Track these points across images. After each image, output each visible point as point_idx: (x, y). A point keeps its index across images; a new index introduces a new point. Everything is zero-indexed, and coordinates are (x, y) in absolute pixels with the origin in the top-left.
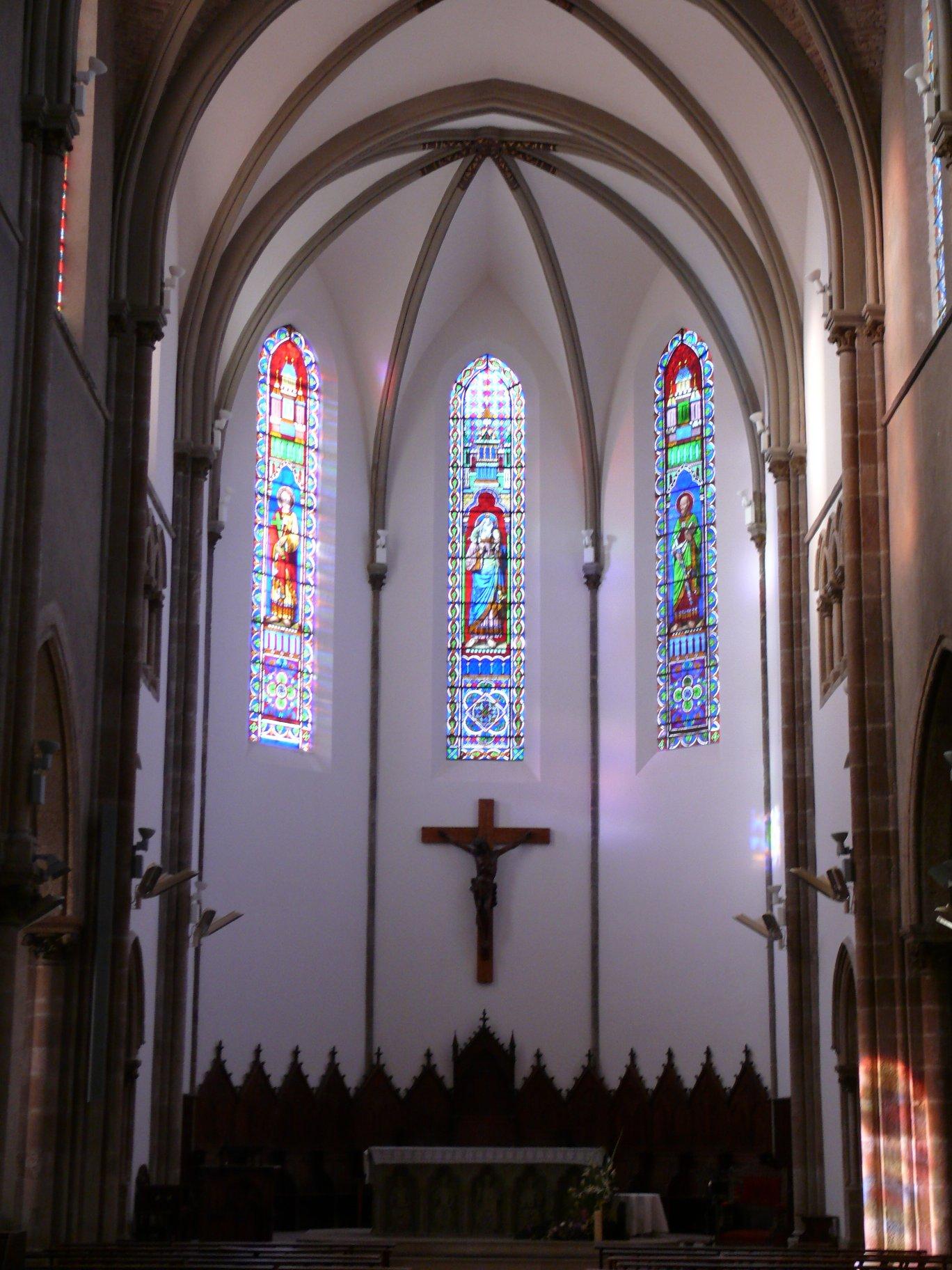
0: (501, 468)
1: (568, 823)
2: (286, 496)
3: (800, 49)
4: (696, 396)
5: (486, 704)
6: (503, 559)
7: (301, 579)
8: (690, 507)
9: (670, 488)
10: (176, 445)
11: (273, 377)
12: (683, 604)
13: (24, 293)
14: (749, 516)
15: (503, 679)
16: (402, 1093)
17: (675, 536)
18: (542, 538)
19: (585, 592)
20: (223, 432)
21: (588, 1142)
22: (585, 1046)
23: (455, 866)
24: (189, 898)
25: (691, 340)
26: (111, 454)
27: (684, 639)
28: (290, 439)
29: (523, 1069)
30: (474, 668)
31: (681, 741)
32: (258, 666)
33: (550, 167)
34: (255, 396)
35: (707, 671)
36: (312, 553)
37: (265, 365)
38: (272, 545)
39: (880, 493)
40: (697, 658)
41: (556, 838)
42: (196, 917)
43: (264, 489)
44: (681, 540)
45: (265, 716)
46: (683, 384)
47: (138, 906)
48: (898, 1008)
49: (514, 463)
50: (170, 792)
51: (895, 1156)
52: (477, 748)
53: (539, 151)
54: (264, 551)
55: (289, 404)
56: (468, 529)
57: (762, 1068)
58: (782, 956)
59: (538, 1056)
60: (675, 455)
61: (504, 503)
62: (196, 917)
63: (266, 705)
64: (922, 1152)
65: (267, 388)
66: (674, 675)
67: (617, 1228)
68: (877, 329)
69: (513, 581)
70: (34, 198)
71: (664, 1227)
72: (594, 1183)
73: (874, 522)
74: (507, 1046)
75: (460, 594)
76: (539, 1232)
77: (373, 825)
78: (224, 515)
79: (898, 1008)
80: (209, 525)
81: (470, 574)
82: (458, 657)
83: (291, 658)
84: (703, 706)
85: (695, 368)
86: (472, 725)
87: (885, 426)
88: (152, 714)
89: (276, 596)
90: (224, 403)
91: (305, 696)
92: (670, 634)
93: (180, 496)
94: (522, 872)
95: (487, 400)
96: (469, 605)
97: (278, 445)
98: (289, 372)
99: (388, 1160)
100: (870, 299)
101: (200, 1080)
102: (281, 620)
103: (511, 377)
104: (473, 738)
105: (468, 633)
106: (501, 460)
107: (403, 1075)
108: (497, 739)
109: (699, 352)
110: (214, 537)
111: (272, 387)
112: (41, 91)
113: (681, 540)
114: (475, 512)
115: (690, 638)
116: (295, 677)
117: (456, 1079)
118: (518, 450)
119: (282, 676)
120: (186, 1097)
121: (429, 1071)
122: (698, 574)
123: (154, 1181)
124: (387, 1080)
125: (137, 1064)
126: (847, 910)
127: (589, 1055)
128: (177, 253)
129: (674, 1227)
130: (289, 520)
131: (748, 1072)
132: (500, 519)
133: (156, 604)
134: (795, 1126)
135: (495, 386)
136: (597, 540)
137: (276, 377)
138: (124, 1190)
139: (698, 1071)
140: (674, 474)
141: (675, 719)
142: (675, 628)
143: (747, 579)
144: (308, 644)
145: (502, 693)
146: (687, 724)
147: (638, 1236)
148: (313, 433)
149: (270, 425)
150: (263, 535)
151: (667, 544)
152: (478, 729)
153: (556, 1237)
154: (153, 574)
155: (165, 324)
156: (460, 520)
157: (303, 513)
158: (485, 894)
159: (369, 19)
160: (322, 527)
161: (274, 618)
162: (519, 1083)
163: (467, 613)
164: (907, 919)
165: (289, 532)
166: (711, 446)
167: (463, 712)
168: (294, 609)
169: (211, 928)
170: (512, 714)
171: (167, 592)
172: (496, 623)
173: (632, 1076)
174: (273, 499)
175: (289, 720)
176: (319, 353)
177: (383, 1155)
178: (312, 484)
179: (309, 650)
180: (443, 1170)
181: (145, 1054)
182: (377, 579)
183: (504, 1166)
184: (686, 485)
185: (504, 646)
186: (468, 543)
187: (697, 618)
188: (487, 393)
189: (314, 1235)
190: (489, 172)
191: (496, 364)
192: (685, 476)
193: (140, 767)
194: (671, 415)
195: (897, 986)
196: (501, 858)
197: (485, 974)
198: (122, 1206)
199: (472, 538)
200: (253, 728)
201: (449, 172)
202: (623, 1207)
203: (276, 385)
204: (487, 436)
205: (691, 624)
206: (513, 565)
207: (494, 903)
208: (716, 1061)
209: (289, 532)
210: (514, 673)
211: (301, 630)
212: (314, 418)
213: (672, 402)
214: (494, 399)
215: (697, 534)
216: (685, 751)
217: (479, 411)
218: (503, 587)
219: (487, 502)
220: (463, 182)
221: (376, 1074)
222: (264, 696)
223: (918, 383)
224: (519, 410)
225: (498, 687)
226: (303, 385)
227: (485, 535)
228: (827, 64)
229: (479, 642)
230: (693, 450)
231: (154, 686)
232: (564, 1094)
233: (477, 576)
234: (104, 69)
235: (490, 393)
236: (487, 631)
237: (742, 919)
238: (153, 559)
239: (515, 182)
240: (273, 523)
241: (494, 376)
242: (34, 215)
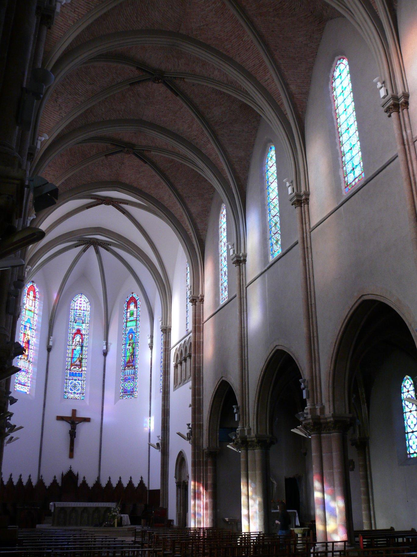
1: (95, 417)
2: (28, 326)
3: (186, 232)
4: (135, 310)
5: (75, 384)
6: (82, 347)
9: (127, 332)
12: (129, 362)
14: (149, 341)
15: (80, 378)
16: (47, 487)
18: (92, 343)
19: (103, 357)
21: (113, 502)
23: (65, 427)
25: (135, 296)
28: (31, 311)
29: (80, 481)
30: (72, 374)
38: (24, 338)
39: (201, 340)
41: (92, 420)
43: (23, 323)
44: (129, 346)
45: (19, 384)
46: (132, 306)
48: (202, 468)
51: (199, 506)
52: (72, 396)
53: (106, 245)
54: (22, 340)
55: (31, 301)
56: (73, 338)
57: (145, 482)
59: (84, 478)
60: (129, 324)
61: (83, 332)
64: (206, 504)
66: (126, 380)
67: (120, 524)
68: (202, 300)
69: (84, 352)
71: (129, 523)
72: (114, 512)
73: (199, 347)
75: (70, 355)
76: (100, 525)
77: (44, 415)
79: (202, 468)
81: (73, 350)
84: (133, 389)
85: (136, 303)
86: (71, 389)
94: (82, 428)
95: (80, 305)
96: (72, 358)
97: (27, 312)
98: (31, 293)
99: (60, 506)
100: (200, 293)
103: (87, 300)
105: (72, 365)
107: (48, 482)
108: (78, 394)
109: (137, 299)
113: (129, 346)
114: (76, 334)
118: (87, 319)
121: (55, 481)
122: (133, 354)
124: (44, 484)
129: (132, 524)
130: (29, 332)
131: (141, 483)
135: (82, 302)
136: (107, 344)
137: (28, 294)
140: (129, 329)
143: (149, 358)
144: (30, 365)
145: (79, 382)
146: (129, 393)
147: (126, 525)
148: (36, 310)
153: (105, 526)
157: (32, 330)
158: (73, 434)
159: (73, 209)
160: (36, 335)
166: (138, 322)
170: (82, 387)
173: (109, 484)
174: (25, 326)
175: (24, 385)
176: (39, 289)
178: (35, 323)
179: (31, 367)
180: (74, 509)
182: (49, 349)
183: (79, 507)
184: (131, 332)
186: (73, 342)
187: (132, 366)
188: (80, 304)
190: (92, 249)
191: (83, 297)
192: (131, 329)
194: (128, 314)
195: (202, 462)
196: (77, 425)
197: (71, 456)
202: (121, 518)
204: (80, 315)
206: (84, 348)
211: (29, 361)
212: (37, 306)
214: (82, 305)
215: (134, 345)
216: (127, 400)
217: (78, 308)
218: (81, 354)
219: (79, 331)
220: (84, 250)
221: (41, 482)
222: (19, 378)
223: (217, 314)
224: (89, 309)
226: (35, 297)
227: (78, 340)
228: (193, 236)
230: (134, 323)
235: (81, 304)
236: (77, 365)
239: (97, 252)
241: (83, 300)
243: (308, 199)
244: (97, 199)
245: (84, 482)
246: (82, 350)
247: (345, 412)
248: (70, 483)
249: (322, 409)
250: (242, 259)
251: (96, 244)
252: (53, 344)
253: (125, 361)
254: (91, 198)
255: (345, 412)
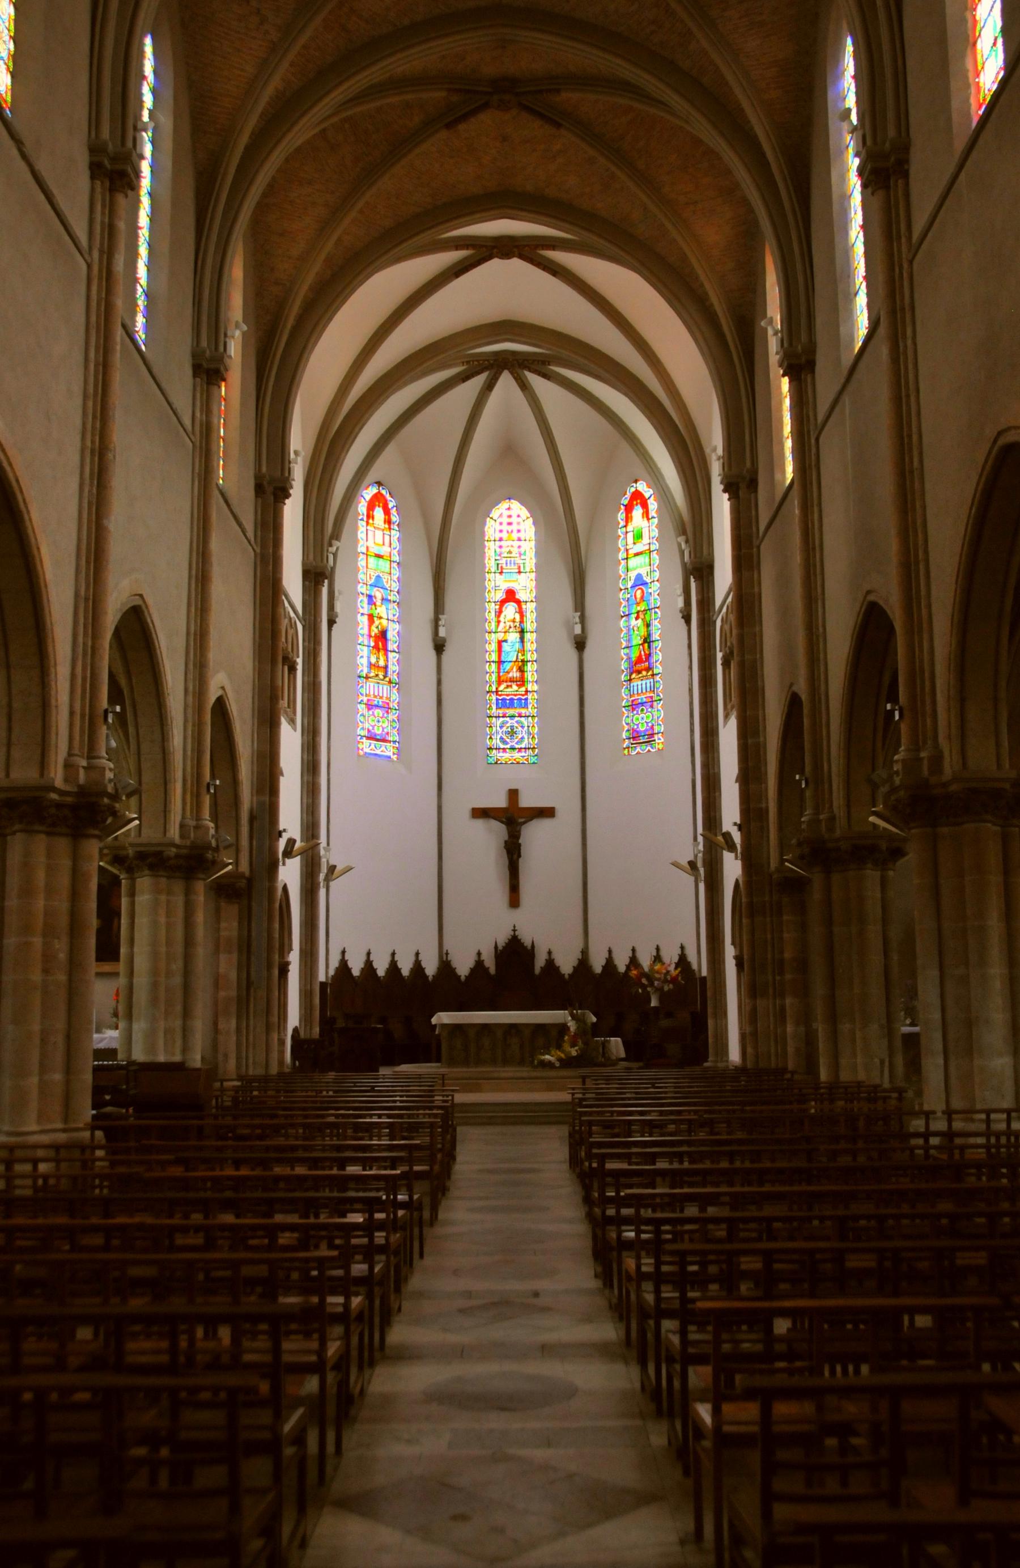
0: (520, 572)
2: (379, 596)
5: (512, 727)
6: (522, 632)
7: (390, 648)
8: (642, 597)
9: (630, 584)
10: (304, 564)
11: (368, 517)
12: (639, 660)
13: (196, 475)
15: (523, 711)
16: (463, 978)
17: (634, 616)
19: (572, 654)
20: (335, 555)
22: (579, 945)
23: (493, 833)
24: (320, 858)
25: (642, 487)
26: (258, 574)
27: (639, 683)
29: (540, 962)
30: (505, 703)
31: (638, 749)
32: (364, 706)
33: (545, 376)
34: (356, 529)
35: (655, 704)
36: (364, 656)
37: (362, 508)
38: (370, 626)
39: (756, 590)
40: (648, 695)
42: (324, 869)
44: (637, 618)
45: (368, 738)
46: (638, 512)
47: (284, 864)
49: (528, 570)
50: (305, 789)
53: (539, 365)
55: (379, 534)
56: (499, 613)
58: (702, 886)
59: (550, 953)
61: (521, 596)
62: (324, 869)
63: (369, 731)
65: (364, 523)
70: (201, 414)
74: (529, 947)
75: (494, 657)
78: (338, 607)
80: (328, 615)
81: (500, 643)
82: (494, 697)
83: (384, 700)
84: (652, 728)
85: (645, 505)
87: (759, 547)
88: (290, 741)
89: (373, 660)
90: (336, 535)
91: (394, 725)
92: (630, 680)
93: (307, 597)
94: (536, 836)
96: (500, 662)
97: (372, 561)
98: (379, 513)
101: (332, 972)
102: (377, 675)
104: (504, 749)
105: (500, 682)
106: (519, 567)
107: (463, 967)
108: (520, 749)
109: (647, 495)
110: (331, 622)
111: (367, 523)
112: (204, 344)
113: (637, 618)
114: (503, 602)
115: (644, 682)
116: (387, 712)
117: (497, 970)
118: (530, 562)
119: (378, 712)
120: (322, 983)
121: (479, 964)
123: (302, 1035)
124: (423, 970)
125: (288, 964)
126: (736, 858)
127: (582, 952)
128: (300, 440)
131: (683, 961)
132: (520, 607)
133: (292, 669)
134: (709, 994)
135: (514, 520)
137: (370, 516)
138: (282, 1042)
139: (603, 962)
140: (633, 575)
141: (635, 735)
142: (634, 676)
145: (523, 719)
149: (367, 548)
150: (364, 620)
151: (628, 621)
152: (507, 743)
154: (290, 649)
155: (292, 487)
156: (493, 607)
157: (391, 606)
158: (513, 850)
161: (372, 674)
162: (537, 970)
163: (499, 668)
164: (773, 864)
165: (381, 618)
167: (497, 732)
168: (386, 668)
169: (334, 876)
171: (299, 661)
172: (518, 674)
173: (610, 964)
174: (370, 597)
177: (443, 1018)
178: (395, 586)
179: (395, 696)
180: (485, 1028)
181: (294, 958)
185: (523, 689)
186: (499, 622)
188: (510, 524)
189: (405, 1068)
190: (506, 380)
192: (639, 577)
193: (282, 775)
194: (630, 536)
197: (514, 902)
198: (282, 1052)
199: (502, 618)
200: (360, 746)
201: (478, 381)
203: (371, 521)
204: (510, 552)
205: (644, 673)
207: (519, 856)
208: (615, 955)
209: (381, 618)
210: (530, 706)
211: (390, 682)
213: (630, 528)
218: (522, 651)
219: (510, 596)
221: (446, 966)
225: (520, 716)
226: (389, 522)
229: (508, 686)
231: (292, 721)
232: (567, 976)
233: (504, 644)
234: (245, 328)
235: (511, 537)
236: (512, 680)
237: (675, 864)
238: (290, 640)
239: (524, 386)
240: (371, 612)
242: (201, 425)
243: (907, 161)
244: (472, 246)
245: (550, 963)
246: (522, 640)
247: (999, 766)
248: (515, 971)
249: (937, 760)
250: (803, 360)
251: (498, 364)
252: (447, 632)
253: (629, 659)
254: (457, 248)
255: (999, 766)
